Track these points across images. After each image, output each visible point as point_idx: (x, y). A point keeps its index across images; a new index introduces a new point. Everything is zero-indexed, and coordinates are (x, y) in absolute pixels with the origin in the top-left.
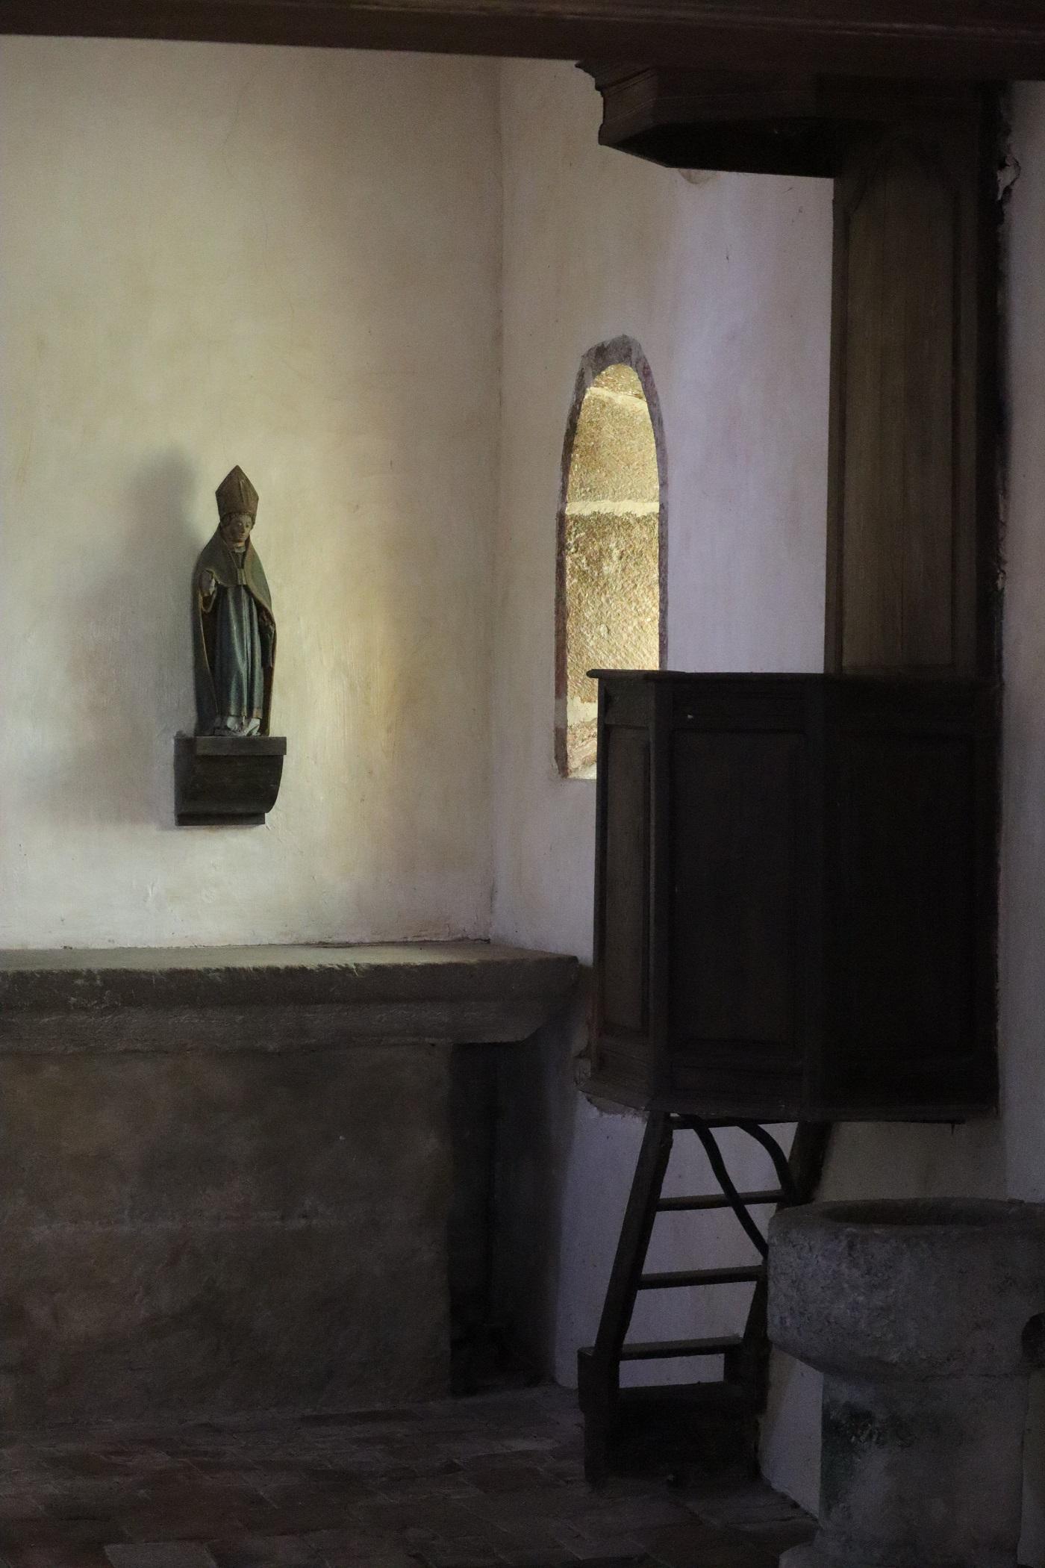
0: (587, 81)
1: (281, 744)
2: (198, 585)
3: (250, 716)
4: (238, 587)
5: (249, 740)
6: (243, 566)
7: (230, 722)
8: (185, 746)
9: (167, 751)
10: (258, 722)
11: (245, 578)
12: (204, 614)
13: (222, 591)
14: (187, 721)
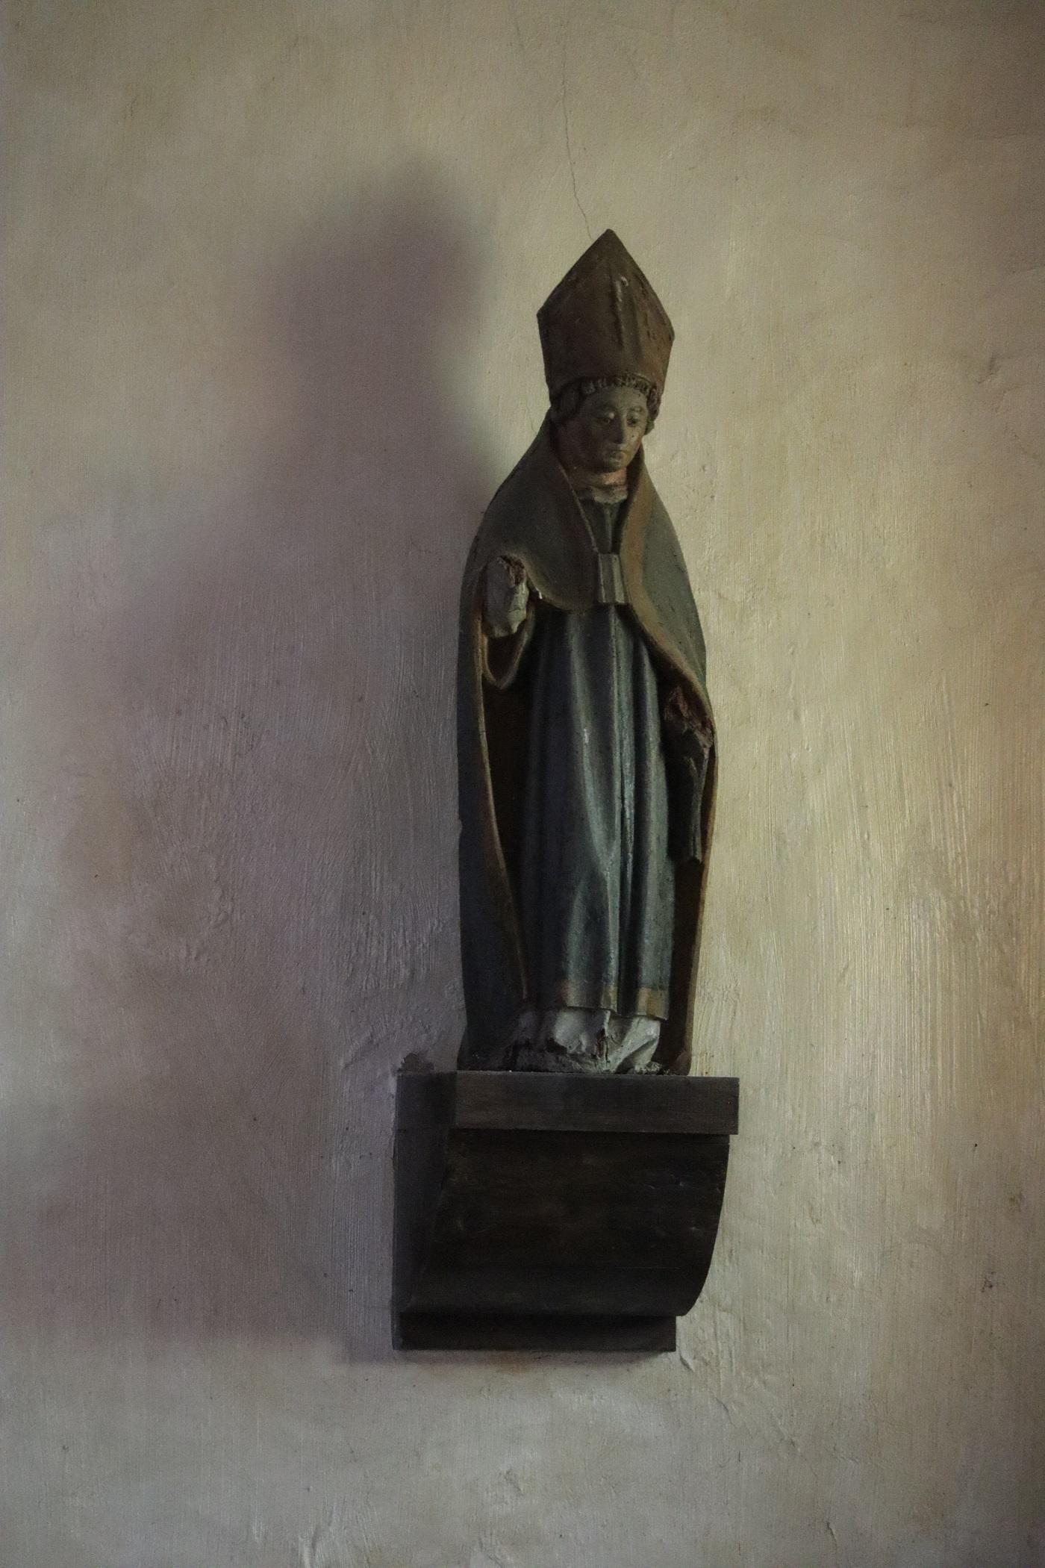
0: (547, 405)
1: (723, 1099)
2: (478, 600)
3: (627, 1011)
4: (600, 611)
5: (622, 1087)
6: (616, 548)
7: (566, 1029)
8: (426, 1095)
9: (373, 1110)
10: (653, 1030)
11: (624, 581)
12: (489, 689)
13: (548, 620)
14: (439, 1025)
